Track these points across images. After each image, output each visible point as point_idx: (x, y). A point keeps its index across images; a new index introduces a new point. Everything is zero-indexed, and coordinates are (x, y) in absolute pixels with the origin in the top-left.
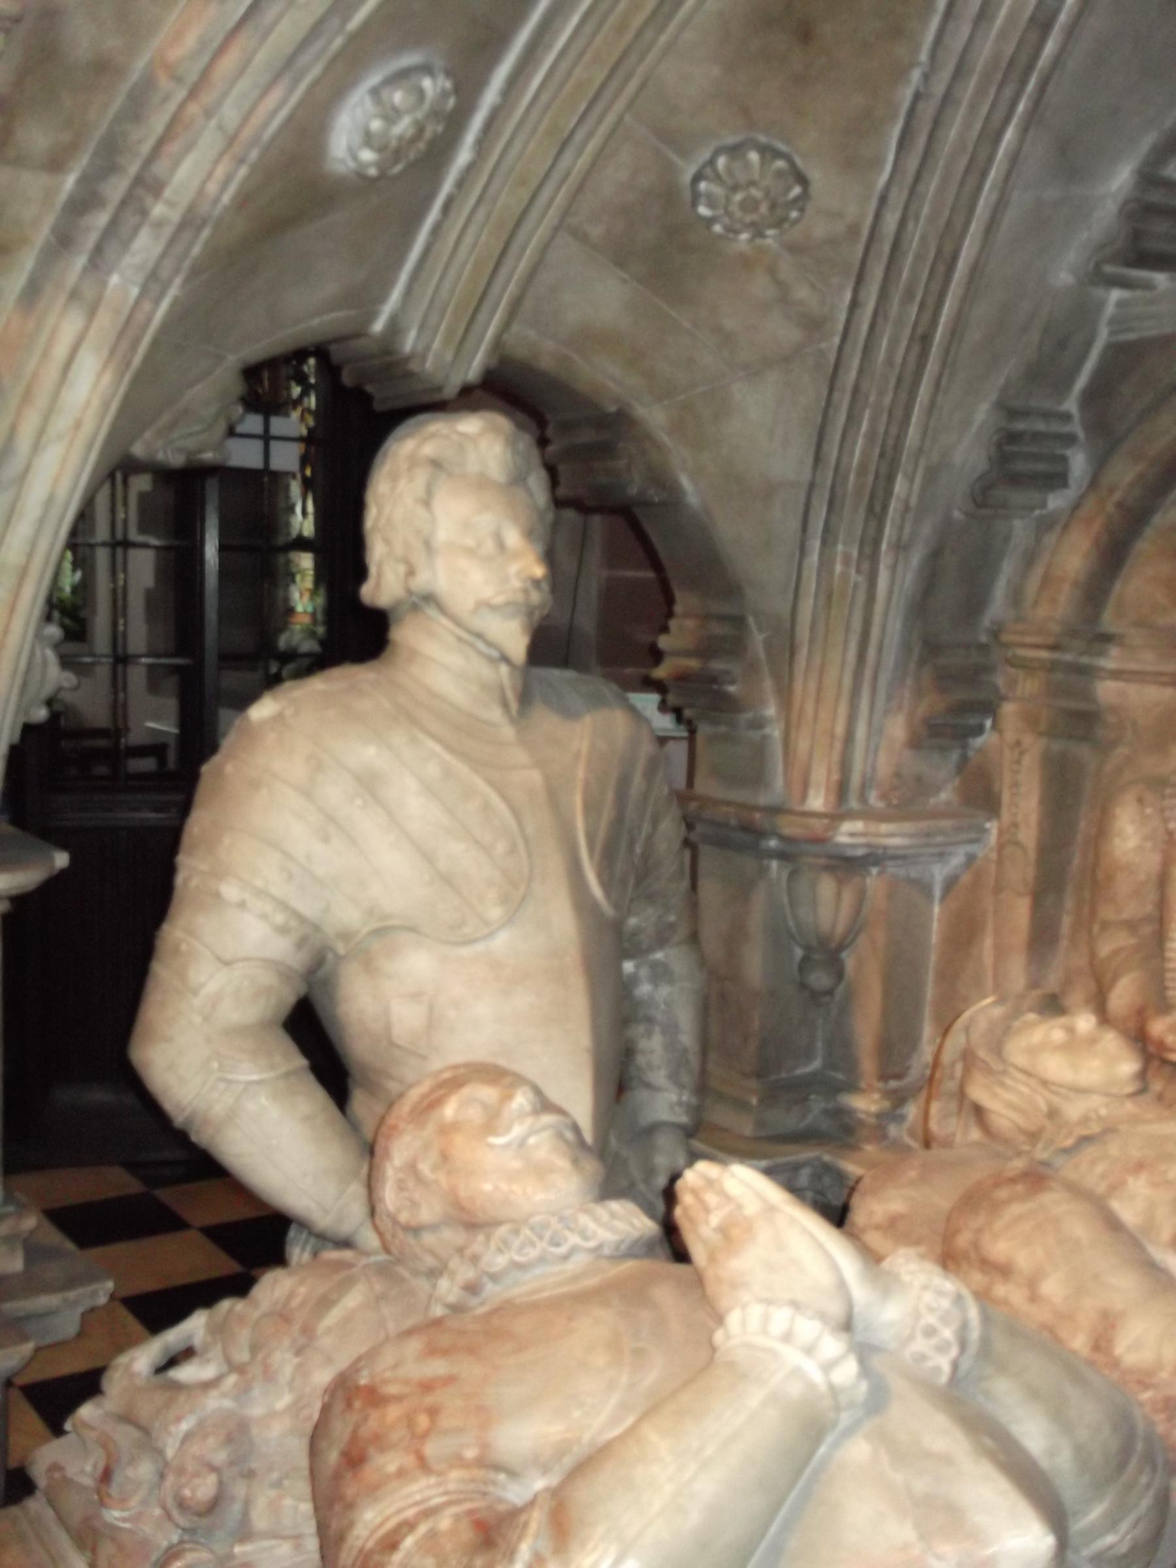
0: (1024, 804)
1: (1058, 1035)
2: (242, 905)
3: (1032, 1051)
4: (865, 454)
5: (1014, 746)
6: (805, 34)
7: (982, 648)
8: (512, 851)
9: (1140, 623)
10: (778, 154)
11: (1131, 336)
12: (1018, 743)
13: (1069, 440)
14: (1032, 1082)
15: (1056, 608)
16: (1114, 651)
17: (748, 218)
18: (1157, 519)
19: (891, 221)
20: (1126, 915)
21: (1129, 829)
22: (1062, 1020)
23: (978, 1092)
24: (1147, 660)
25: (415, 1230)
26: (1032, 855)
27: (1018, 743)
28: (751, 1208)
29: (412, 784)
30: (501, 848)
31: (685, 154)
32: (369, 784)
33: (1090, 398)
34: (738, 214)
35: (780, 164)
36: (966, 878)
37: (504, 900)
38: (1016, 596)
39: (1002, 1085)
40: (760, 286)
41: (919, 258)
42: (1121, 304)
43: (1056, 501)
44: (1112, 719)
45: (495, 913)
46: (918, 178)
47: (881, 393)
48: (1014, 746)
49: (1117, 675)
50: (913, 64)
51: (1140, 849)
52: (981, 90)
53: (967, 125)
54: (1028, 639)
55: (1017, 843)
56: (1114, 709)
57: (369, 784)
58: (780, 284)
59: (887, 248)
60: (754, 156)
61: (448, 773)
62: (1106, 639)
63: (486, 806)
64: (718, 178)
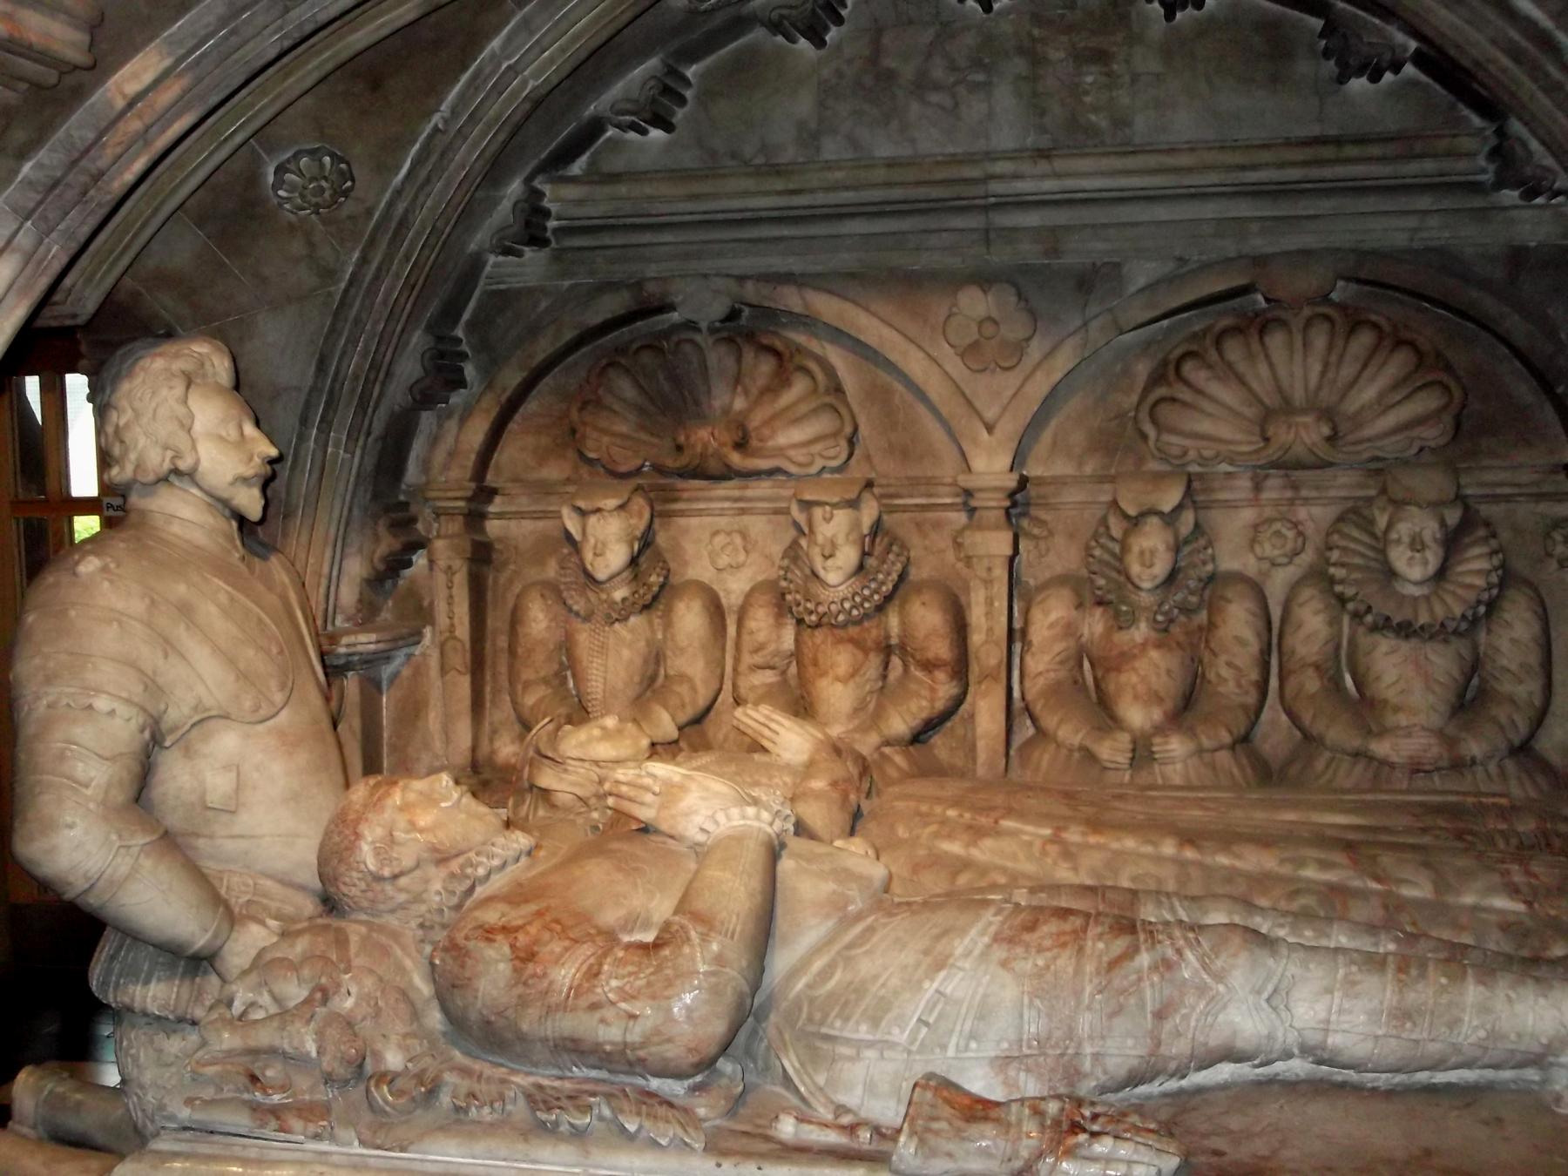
0: (452, 610)
1: (596, 732)
2: (112, 713)
3: (581, 745)
4: (359, 366)
5: (439, 573)
6: (376, 84)
7: (406, 505)
8: (281, 652)
9: (516, 480)
10: (342, 160)
11: (502, 287)
12: (450, 567)
13: (463, 356)
14: (587, 765)
15: (460, 474)
16: (498, 499)
17: (314, 200)
18: (521, 410)
19: (401, 207)
20: (542, 674)
21: (541, 616)
22: (593, 724)
23: (547, 779)
24: (524, 503)
25: (1138, 588)
26: (468, 645)
27: (450, 567)
28: (677, 779)
29: (213, 609)
30: (275, 650)
31: (271, 151)
32: (185, 610)
33: (472, 326)
34: (309, 197)
35: (343, 166)
36: (406, 672)
37: (282, 687)
38: (426, 466)
39: (566, 771)
40: (297, 247)
41: (419, 234)
42: (496, 265)
43: (457, 398)
44: (498, 546)
45: (279, 698)
46: (428, 180)
47: (376, 322)
48: (439, 573)
49: (500, 516)
50: (438, 111)
51: (548, 628)
52: (484, 134)
53: (470, 153)
54: (450, 494)
55: (455, 638)
56: (500, 540)
57: (185, 610)
58: (311, 245)
59: (393, 225)
60: (327, 159)
61: (232, 599)
62: (493, 492)
63: (260, 620)
64: (300, 173)
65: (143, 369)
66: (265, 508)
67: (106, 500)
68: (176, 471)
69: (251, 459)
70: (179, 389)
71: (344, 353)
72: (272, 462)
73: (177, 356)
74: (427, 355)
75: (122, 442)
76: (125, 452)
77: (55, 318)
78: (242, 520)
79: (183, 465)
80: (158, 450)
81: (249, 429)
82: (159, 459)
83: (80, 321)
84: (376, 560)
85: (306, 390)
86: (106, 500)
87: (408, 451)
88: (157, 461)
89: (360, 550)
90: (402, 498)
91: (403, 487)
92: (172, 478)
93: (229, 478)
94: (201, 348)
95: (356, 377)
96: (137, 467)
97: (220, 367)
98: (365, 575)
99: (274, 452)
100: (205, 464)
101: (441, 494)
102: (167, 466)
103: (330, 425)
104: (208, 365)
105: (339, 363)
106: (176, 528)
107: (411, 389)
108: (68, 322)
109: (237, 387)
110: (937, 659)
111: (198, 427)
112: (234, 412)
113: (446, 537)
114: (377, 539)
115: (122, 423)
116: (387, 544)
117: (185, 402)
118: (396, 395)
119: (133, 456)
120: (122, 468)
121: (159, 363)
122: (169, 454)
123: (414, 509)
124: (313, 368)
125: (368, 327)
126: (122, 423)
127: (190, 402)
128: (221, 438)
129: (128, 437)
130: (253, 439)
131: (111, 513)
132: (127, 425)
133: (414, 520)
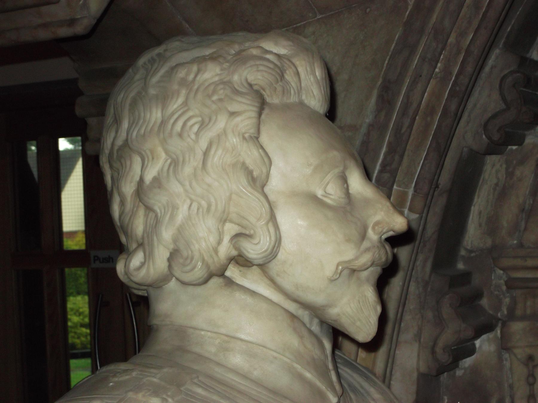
12: (531, 358)
47: (462, 35)
65: (183, 83)
66: (383, 319)
67: (93, 253)
68: (241, 261)
69: (363, 236)
70: (245, 122)
71: (417, 77)
72: (395, 241)
73: (241, 59)
74: (509, 80)
75: (149, 209)
76: (154, 226)
77: (45, 25)
78: (337, 335)
79: (254, 250)
81: (357, 183)
82: (213, 239)
83: (80, 29)
84: (439, 350)
85: (363, 130)
86: (93, 253)
87: (469, 210)
88: (208, 239)
89: (418, 337)
90: (461, 266)
91: (463, 253)
92: (232, 272)
93: (329, 270)
94: (276, 47)
95: (431, 111)
96: (174, 255)
97: (309, 85)
98: (423, 369)
99: (399, 223)
100: (289, 246)
101: (519, 262)
102: (225, 250)
103: (394, 174)
105: (411, 89)
107: (485, 126)
108: (64, 32)
109: (331, 114)
111: (276, 184)
113: (523, 318)
114: (440, 322)
115: (149, 177)
116: (452, 331)
117: (255, 139)
118: (468, 135)
119: (167, 234)
120: (149, 256)
121: (211, 73)
122: (230, 229)
123: (476, 280)
124: (373, 100)
126: (149, 177)
127: (264, 139)
128: (314, 199)
129: (158, 201)
130: (367, 202)
131: (97, 265)
132: (157, 181)
133: (479, 295)
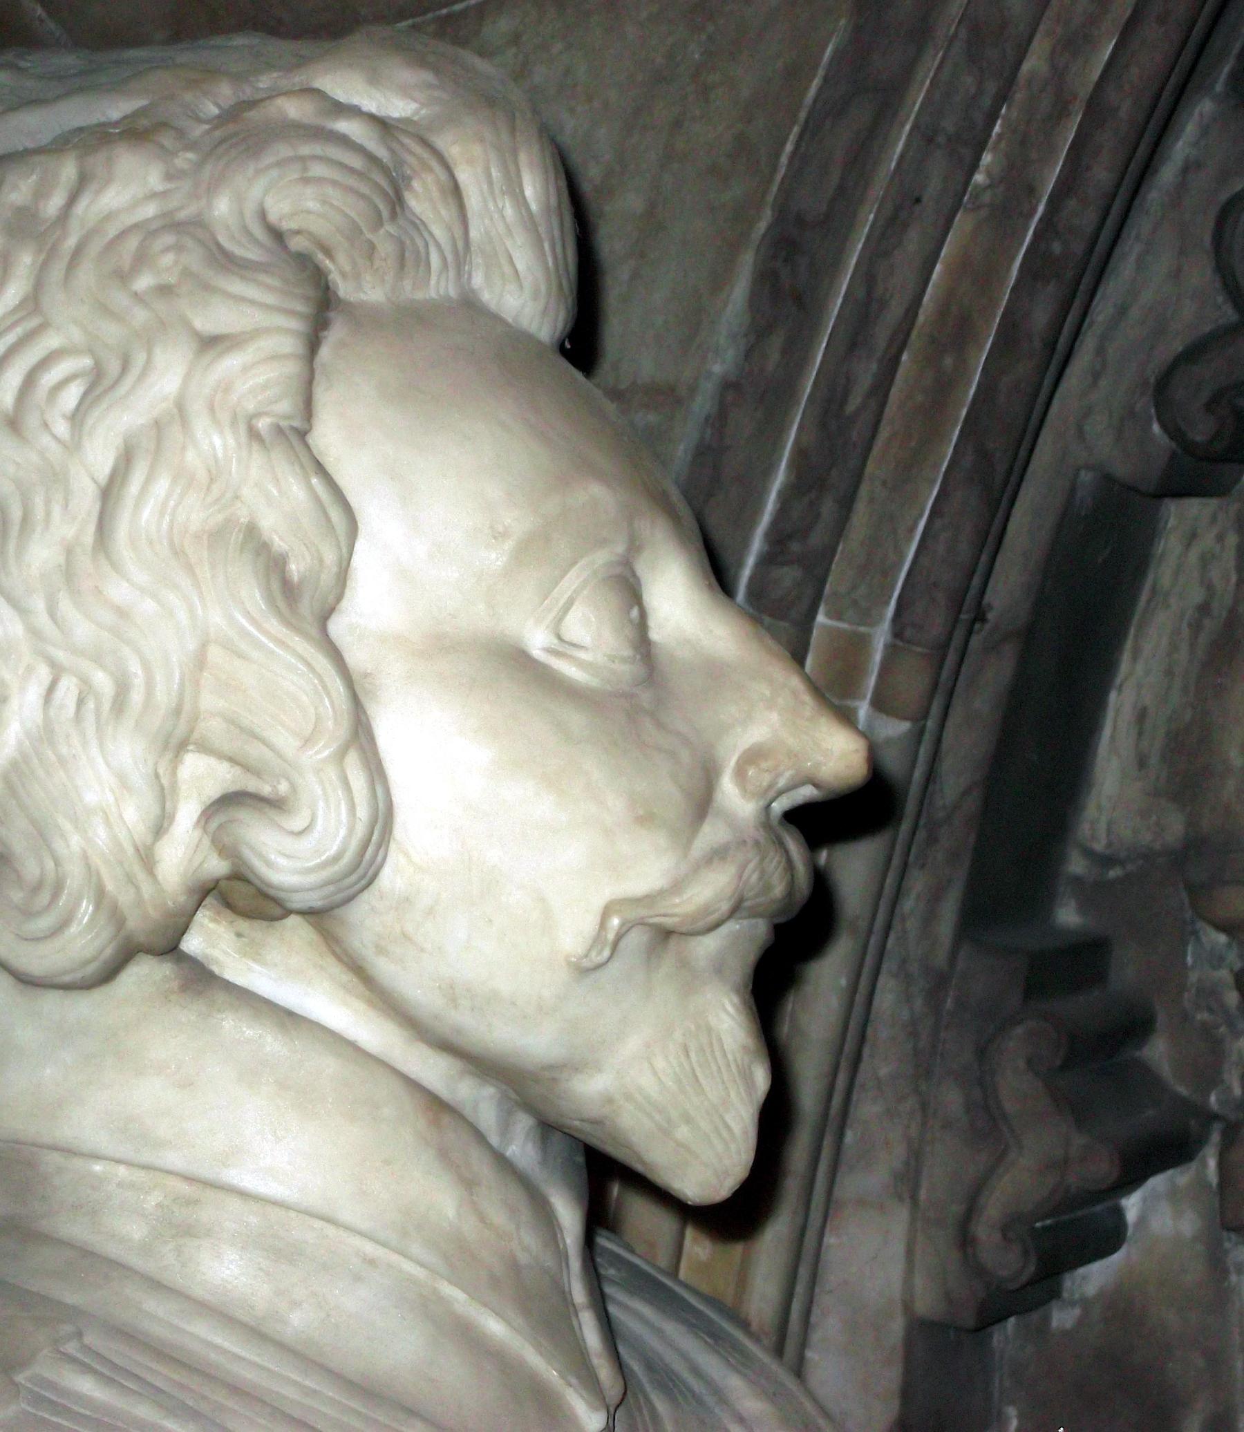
4: (978, 273)
47: (1074, 43)
66: (775, 1118)
68: (243, 896)
69: (702, 803)
70: (257, 372)
71: (905, 203)
72: (823, 820)
73: (242, 136)
78: (606, 1177)
79: (290, 856)
80: (129, 751)
81: (677, 601)
82: (134, 816)
84: (985, 1231)
85: (703, 403)
89: (908, 1182)
90: (1068, 916)
91: (1076, 865)
92: (210, 938)
93: (574, 931)
95: (956, 331)
98: (927, 1303)
102: (182, 855)
103: (816, 569)
104: (423, 200)
105: (879, 250)
106: (226, 1269)
107: (1162, 388)
109: (581, 344)
110: (181, 762)
111: (374, 608)
112: (598, 496)
117: (296, 436)
121: (130, 189)
122: (202, 776)
123: (1128, 969)
124: (740, 290)
125: (1035, 63)
127: (328, 436)
130: (715, 673)
